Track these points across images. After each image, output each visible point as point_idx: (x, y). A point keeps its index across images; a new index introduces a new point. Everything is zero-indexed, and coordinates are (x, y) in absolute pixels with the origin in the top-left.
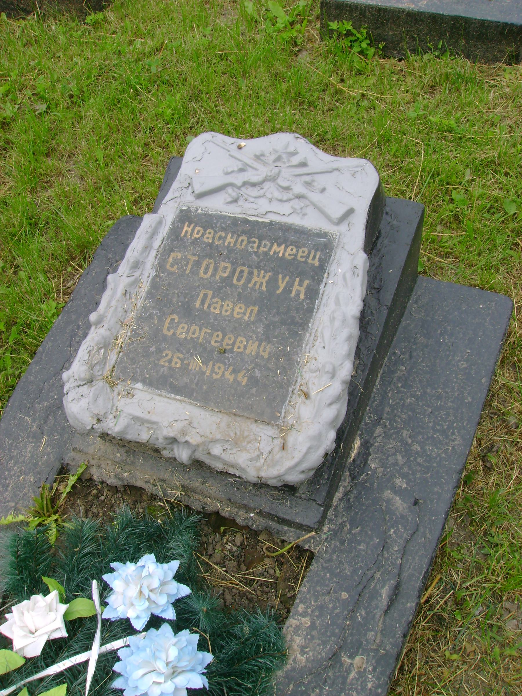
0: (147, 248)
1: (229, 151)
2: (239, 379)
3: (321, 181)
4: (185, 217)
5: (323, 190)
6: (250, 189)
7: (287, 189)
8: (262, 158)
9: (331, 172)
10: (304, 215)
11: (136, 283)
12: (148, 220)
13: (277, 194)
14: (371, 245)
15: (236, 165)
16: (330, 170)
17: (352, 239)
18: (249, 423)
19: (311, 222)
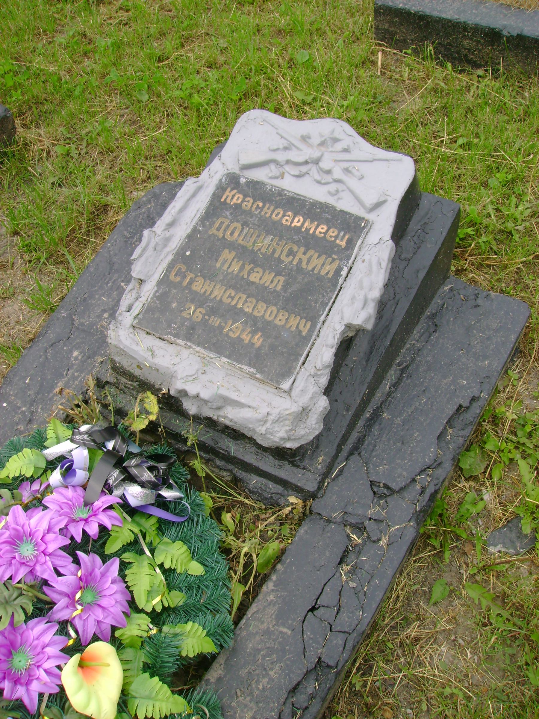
1: (276, 129)
2: (255, 340)
4: (232, 181)
5: (362, 178)
7: (329, 172)
8: (307, 140)
12: (190, 184)
14: (398, 234)
15: (282, 143)
17: (384, 223)
19: (346, 204)
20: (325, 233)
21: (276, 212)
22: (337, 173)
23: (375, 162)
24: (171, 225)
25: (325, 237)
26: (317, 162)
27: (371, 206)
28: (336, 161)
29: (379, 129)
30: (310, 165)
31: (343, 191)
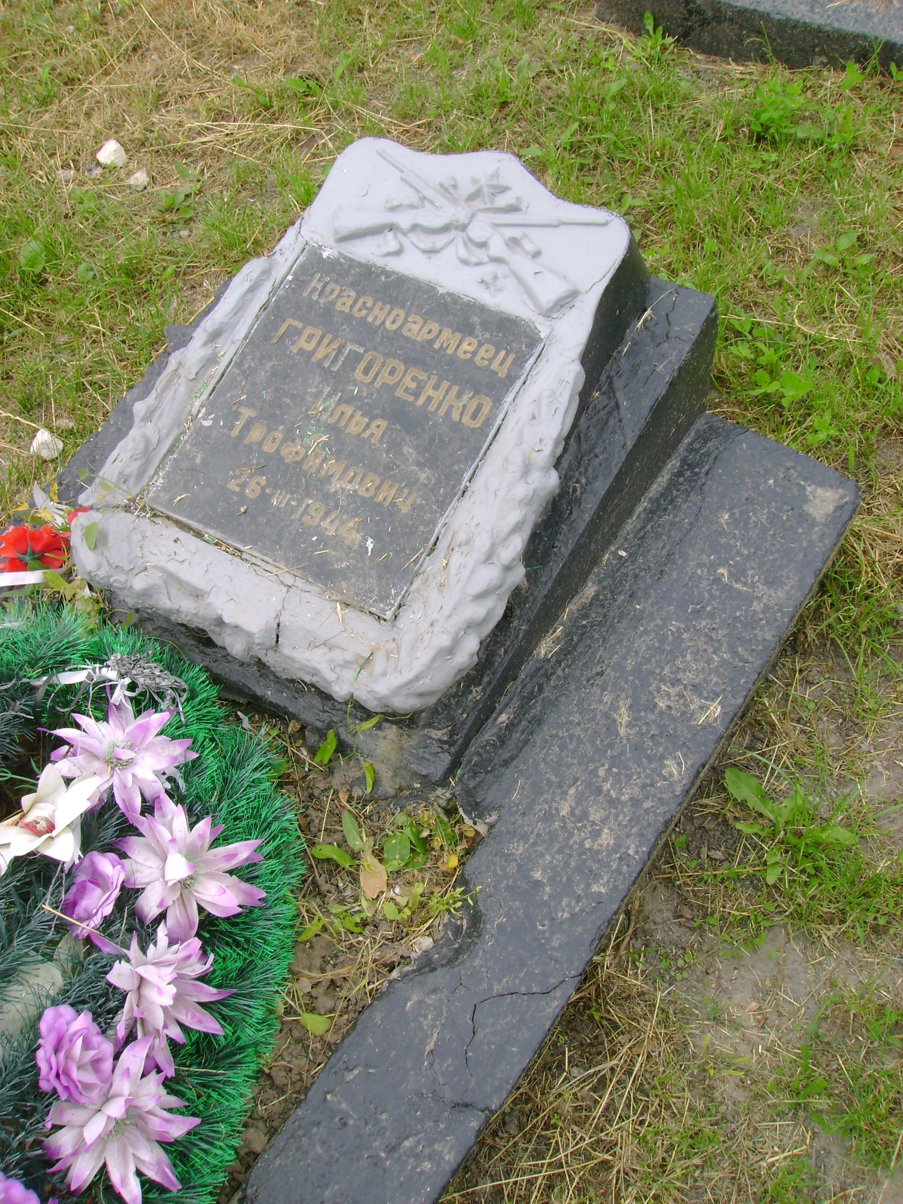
0: (239, 309)
3: (537, 239)
5: (537, 254)
6: (422, 236)
7: (483, 245)
9: (556, 226)
10: (500, 290)
11: (212, 360)
12: (253, 268)
13: (463, 253)
15: (410, 196)
16: (555, 223)
17: (574, 330)
18: (684, 782)
19: (507, 301)
20: (474, 353)
21: (394, 313)
22: (497, 247)
23: (562, 228)
24: (215, 336)
25: (471, 359)
26: (463, 228)
27: (550, 305)
28: (497, 225)
29: (583, 169)
30: (453, 234)
31: (506, 277)
